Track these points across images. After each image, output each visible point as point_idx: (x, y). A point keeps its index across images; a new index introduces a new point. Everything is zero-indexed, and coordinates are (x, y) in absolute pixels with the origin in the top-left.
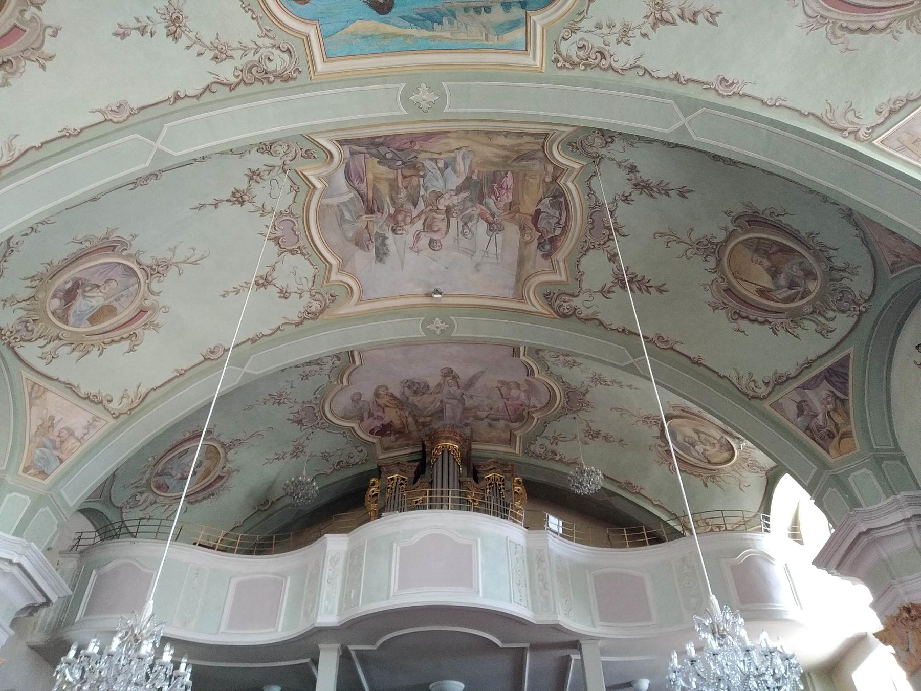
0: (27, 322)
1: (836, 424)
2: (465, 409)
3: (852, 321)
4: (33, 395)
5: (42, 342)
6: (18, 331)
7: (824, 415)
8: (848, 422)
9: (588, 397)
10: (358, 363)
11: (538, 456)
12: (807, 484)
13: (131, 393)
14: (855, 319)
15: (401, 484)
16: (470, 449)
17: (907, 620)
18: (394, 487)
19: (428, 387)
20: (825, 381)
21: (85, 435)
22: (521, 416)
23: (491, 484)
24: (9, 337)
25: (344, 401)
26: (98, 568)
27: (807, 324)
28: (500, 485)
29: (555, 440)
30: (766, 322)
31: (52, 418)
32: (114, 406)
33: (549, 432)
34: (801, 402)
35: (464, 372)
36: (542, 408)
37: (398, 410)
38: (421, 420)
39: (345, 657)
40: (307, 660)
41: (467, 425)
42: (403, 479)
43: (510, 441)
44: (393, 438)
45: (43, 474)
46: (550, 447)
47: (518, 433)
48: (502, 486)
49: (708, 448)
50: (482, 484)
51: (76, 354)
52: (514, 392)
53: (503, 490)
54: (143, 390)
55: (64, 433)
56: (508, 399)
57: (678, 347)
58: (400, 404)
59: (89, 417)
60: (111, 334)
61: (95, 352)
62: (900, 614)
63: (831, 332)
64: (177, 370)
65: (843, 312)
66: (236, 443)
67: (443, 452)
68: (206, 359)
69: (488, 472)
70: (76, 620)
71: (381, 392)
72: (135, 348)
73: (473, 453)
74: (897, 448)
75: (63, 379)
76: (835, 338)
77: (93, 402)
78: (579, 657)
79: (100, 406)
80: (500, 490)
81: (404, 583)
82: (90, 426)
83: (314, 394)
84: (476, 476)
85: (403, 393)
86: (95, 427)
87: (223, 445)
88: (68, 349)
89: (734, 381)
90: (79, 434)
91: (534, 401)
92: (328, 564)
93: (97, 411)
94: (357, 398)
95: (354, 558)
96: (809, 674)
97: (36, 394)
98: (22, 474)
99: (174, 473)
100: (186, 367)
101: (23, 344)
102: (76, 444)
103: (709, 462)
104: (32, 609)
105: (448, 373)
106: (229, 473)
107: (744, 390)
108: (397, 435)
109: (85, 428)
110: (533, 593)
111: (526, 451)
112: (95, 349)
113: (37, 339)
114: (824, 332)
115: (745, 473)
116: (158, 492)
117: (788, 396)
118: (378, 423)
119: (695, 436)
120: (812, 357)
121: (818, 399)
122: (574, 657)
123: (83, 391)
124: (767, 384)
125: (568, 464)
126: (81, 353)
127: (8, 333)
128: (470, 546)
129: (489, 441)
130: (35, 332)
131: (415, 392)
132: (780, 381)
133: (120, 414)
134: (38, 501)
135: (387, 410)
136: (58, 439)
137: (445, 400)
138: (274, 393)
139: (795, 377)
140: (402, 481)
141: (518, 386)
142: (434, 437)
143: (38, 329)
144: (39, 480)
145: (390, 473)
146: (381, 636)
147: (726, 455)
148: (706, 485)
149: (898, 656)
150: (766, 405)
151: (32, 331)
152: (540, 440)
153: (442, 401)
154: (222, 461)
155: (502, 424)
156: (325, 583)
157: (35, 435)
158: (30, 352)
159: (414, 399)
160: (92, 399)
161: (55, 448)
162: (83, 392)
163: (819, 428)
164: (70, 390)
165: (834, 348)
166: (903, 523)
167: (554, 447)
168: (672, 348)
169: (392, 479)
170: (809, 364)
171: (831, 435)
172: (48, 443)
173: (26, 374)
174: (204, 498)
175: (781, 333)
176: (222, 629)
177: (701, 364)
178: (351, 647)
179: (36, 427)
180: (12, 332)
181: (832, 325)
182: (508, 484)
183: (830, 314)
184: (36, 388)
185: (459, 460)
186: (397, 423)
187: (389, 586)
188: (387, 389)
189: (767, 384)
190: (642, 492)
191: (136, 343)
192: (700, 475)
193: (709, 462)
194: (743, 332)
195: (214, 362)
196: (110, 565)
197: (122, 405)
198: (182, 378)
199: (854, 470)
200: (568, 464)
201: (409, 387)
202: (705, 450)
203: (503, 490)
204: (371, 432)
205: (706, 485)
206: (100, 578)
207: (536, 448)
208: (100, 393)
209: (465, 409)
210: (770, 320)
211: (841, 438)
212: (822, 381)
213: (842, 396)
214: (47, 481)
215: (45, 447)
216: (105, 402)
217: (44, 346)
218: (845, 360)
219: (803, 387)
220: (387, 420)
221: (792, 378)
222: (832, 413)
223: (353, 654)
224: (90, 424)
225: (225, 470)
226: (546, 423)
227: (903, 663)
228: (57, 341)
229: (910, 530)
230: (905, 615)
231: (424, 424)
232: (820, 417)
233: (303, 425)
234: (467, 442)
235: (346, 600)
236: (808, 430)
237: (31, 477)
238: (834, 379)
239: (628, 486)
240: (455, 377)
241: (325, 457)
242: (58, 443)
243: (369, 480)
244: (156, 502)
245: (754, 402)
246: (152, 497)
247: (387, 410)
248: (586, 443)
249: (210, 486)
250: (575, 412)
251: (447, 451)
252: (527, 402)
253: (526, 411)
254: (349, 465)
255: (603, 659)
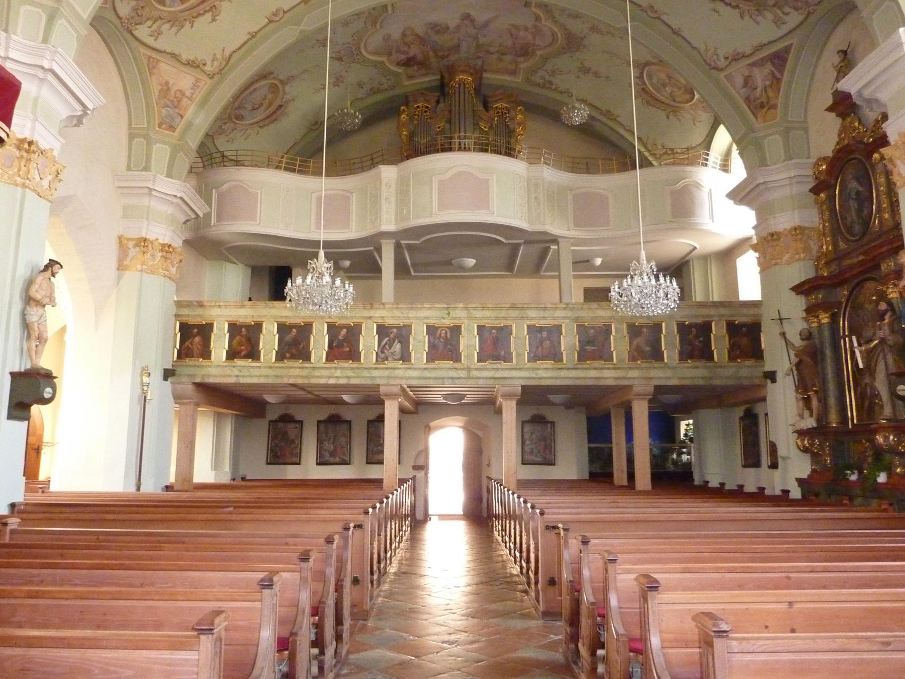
0: (138, 9)
1: (768, 97)
2: (478, 46)
3: (801, 18)
4: (151, 66)
5: (149, 23)
6: (133, 17)
7: (762, 91)
8: (777, 97)
9: (586, 42)
10: (390, 12)
11: (538, 85)
12: (737, 138)
13: (219, 56)
14: (804, 17)
15: (426, 112)
16: (481, 78)
17: (770, 240)
18: (420, 114)
19: (448, 28)
20: (769, 63)
21: (193, 94)
22: (525, 51)
23: (498, 112)
24: (127, 23)
25: (376, 40)
26: (216, 188)
27: (768, 15)
28: (506, 113)
29: (553, 73)
30: (737, 7)
31: (167, 83)
32: (208, 68)
33: (549, 66)
34: (748, 76)
35: (481, 17)
36: (546, 47)
37: (421, 46)
38: (440, 54)
39: (398, 247)
40: (372, 248)
41: (479, 58)
42: (427, 107)
43: (513, 73)
44: (416, 68)
45: (172, 128)
46: (547, 78)
47: (523, 66)
48: (507, 115)
49: (675, 90)
50: (491, 112)
51: (174, 29)
52: (522, 33)
53: (508, 118)
54: (227, 54)
55: (178, 94)
56: (516, 39)
57: (664, 18)
58: (422, 41)
59: (193, 80)
60: (197, 9)
61: (187, 25)
62: (767, 237)
63: (784, 24)
64: (249, 33)
65: (796, 9)
66: (291, 78)
67: (459, 85)
68: (270, 22)
69: (497, 101)
70: (212, 224)
71: (408, 33)
72: (216, 18)
73: (484, 81)
74: (805, 121)
75: (169, 50)
76: (785, 29)
77: (192, 66)
78: (556, 247)
79: (198, 69)
80: (506, 118)
81: (442, 206)
82: (195, 86)
83: (353, 36)
84: (486, 106)
85: (427, 33)
86: (198, 87)
87: (281, 82)
88: (167, 26)
89: (702, 51)
90: (188, 93)
91: (538, 41)
92: (383, 187)
93: (196, 73)
94: (386, 39)
95: (403, 183)
96: (710, 256)
97: (152, 66)
98: (158, 129)
99: (247, 106)
100: (256, 29)
101: (137, 27)
102: (188, 103)
103: (674, 101)
104: (188, 220)
105: (467, 17)
106: (287, 102)
107: (709, 61)
108: (419, 66)
109: (192, 89)
110: (529, 210)
111: (528, 81)
112: (187, 23)
113: (146, 22)
114: (778, 22)
115: (700, 112)
116: (237, 122)
117: (739, 70)
118: (404, 57)
119: (667, 81)
120: (765, 41)
121: (760, 77)
122: (552, 247)
123: (185, 57)
124: (726, 58)
125: (562, 93)
126: (178, 28)
127: (126, 21)
128: (487, 181)
129: (497, 72)
130: (144, 16)
131: (438, 32)
132: (737, 58)
133: (214, 74)
134: (175, 150)
135: (413, 46)
136: (175, 100)
137: (462, 38)
138: (320, 39)
139: (751, 55)
140: (426, 109)
141: (526, 29)
142: (452, 70)
143: (146, 12)
144: (171, 133)
145: (416, 101)
146: (423, 236)
147: (688, 97)
148: (668, 117)
149: (758, 259)
150: (722, 75)
151: (142, 16)
152: (541, 73)
153: (459, 39)
154: (281, 93)
155: (508, 58)
156: (383, 201)
157: (159, 98)
158: (142, 32)
159: (435, 38)
160: (193, 65)
161: (176, 107)
162: (184, 59)
163: (756, 99)
164: (174, 59)
165: (781, 38)
166: (788, 179)
167: (552, 79)
168: (659, 18)
169: (418, 107)
170: (761, 47)
171: (762, 106)
172: (169, 103)
173: (143, 50)
174: (269, 123)
175: (747, 18)
176: (312, 230)
177: (679, 35)
178: (402, 242)
179: (158, 91)
180: (128, 19)
181: (786, 18)
182: (512, 113)
183: (787, 10)
184: (151, 60)
185: (472, 92)
186: (420, 57)
187: (431, 208)
188: (413, 30)
189: (726, 58)
190: (619, 119)
191: (216, 14)
192: (665, 110)
193: (674, 101)
194: (718, 12)
195: (277, 24)
196: (226, 185)
197: (214, 67)
198: (254, 40)
199: (770, 135)
200: (562, 93)
201: (432, 28)
202: (673, 91)
203: (508, 118)
204: (398, 64)
205: (668, 117)
206: (220, 196)
207: (537, 78)
208: (196, 59)
209: (478, 46)
210: (740, 6)
211: (769, 109)
212: (767, 61)
213: (779, 76)
214: (176, 134)
215: (168, 107)
216: (201, 66)
217: (152, 26)
218: (787, 49)
219: (753, 64)
220: (411, 54)
221: (746, 57)
222: (767, 88)
223: (404, 246)
224: (194, 85)
225: (284, 100)
226: (545, 59)
227: (760, 264)
228: (160, 21)
229: (791, 184)
230: (770, 238)
231: (442, 57)
232: (759, 90)
233: (343, 61)
234: (478, 73)
235: (400, 215)
236: (747, 100)
237: (163, 131)
238: (776, 62)
239: (608, 114)
240: (472, 21)
241: (360, 85)
242: (176, 103)
243: (400, 108)
244: (236, 129)
245: (714, 72)
246: (233, 125)
247: (413, 46)
248: (578, 77)
249: (274, 112)
250: (572, 52)
251: (462, 83)
252: (532, 42)
253: (530, 49)
254: (379, 91)
255: (573, 248)
